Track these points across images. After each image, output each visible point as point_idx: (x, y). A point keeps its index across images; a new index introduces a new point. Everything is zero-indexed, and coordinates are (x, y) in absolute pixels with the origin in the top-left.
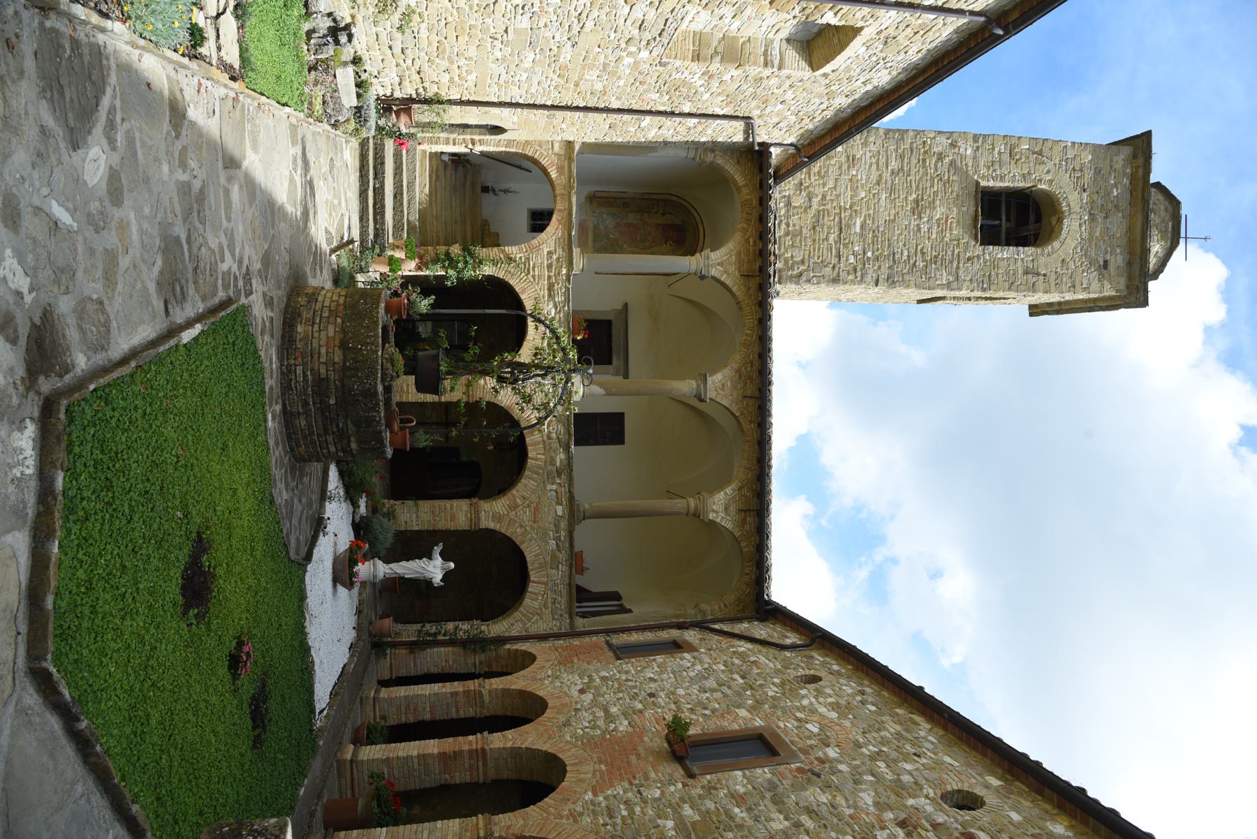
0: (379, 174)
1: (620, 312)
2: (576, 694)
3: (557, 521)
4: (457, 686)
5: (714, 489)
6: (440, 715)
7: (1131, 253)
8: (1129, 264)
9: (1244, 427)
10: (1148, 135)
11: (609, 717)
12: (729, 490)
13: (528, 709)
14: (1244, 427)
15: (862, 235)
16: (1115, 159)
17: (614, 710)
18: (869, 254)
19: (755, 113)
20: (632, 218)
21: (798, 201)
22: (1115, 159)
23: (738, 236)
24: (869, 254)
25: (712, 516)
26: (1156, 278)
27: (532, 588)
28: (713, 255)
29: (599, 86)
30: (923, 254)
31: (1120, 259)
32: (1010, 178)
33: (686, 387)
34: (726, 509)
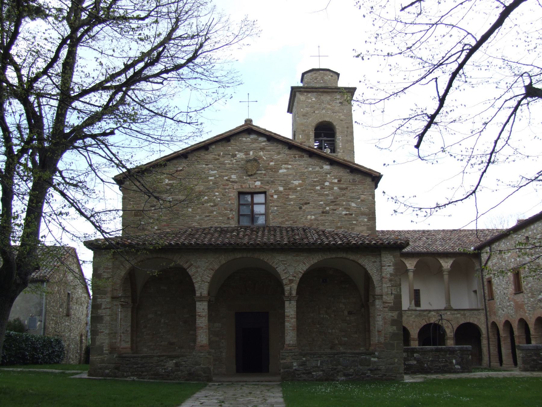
2: (503, 313)
3: (451, 314)
4: (502, 343)
5: (441, 266)
6: (510, 347)
9: (382, 175)
10: (355, 89)
11: (510, 306)
12: (441, 262)
13: (508, 324)
14: (382, 175)
16: (302, 100)
17: (508, 304)
22: (302, 100)
25: (449, 267)
27: (471, 321)
34: (447, 262)
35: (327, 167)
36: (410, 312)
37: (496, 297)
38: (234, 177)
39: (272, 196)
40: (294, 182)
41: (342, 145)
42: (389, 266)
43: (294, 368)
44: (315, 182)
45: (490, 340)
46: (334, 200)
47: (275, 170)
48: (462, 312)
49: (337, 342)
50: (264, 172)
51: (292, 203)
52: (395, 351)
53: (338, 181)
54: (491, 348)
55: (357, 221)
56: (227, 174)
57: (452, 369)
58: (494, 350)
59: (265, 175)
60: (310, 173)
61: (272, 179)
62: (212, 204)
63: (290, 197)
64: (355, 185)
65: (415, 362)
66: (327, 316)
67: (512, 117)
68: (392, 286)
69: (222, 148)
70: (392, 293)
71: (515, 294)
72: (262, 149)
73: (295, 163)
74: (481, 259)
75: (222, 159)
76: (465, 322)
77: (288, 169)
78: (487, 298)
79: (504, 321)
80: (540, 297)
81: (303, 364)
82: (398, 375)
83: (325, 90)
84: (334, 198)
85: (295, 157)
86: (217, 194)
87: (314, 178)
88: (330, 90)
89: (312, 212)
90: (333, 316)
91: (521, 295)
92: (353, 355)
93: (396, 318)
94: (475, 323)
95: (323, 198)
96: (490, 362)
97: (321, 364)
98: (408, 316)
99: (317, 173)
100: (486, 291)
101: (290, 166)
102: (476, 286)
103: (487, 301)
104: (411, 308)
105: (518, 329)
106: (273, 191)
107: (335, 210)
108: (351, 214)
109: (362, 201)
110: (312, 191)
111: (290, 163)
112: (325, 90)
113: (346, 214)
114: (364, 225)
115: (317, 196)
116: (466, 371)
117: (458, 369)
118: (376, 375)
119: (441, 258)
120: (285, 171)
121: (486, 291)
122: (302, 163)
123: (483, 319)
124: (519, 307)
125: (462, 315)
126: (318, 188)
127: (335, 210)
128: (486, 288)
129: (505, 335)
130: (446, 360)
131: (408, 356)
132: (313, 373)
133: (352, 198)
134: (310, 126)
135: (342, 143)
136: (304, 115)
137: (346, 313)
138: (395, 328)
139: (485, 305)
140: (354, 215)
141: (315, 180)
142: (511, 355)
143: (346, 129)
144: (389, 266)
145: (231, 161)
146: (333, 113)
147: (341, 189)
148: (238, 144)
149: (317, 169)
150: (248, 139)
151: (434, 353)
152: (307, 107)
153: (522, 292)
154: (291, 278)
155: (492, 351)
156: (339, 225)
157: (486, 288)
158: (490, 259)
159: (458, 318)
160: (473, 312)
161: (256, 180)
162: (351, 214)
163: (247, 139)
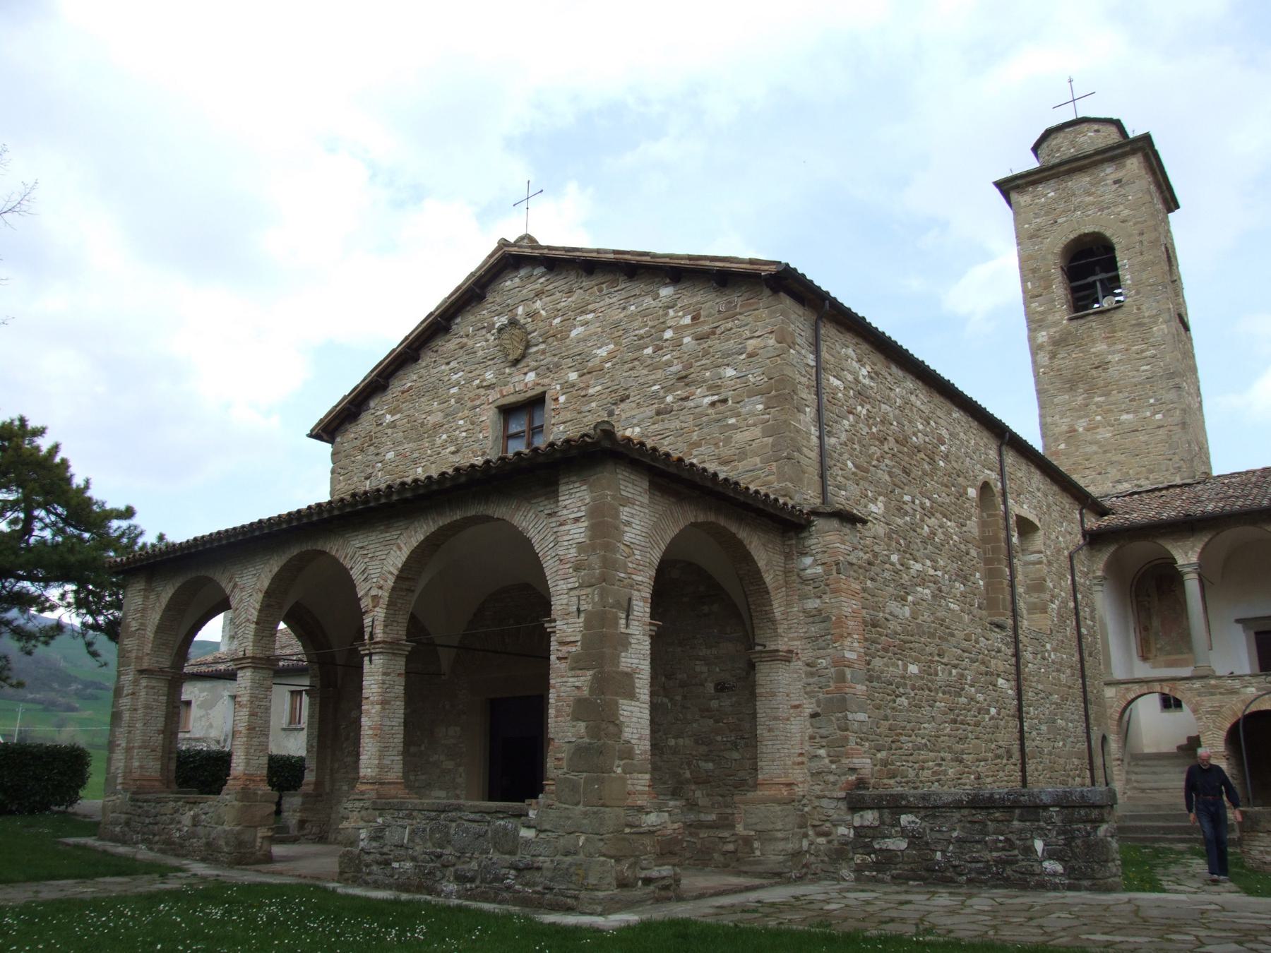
0: (1143, 829)
1: (1246, 629)
7: (1102, 161)
8: (1111, 159)
10: (998, 184)
15: (1135, 412)
16: (1023, 204)
18: (1152, 401)
19: (1066, 553)
20: (1156, 623)
21: (1113, 473)
22: (1023, 204)
23: (1161, 542)
24: (1152, 401)
26: (1117, 124)
29: (1068, 671)
30: (1142, 351)
31: (1109, 170)
32: (1059, 289)
35: (666, 292)
38: (489, 376)
39: (557, 399)
40: (598, 351)
41: (1132, 279)
42: (577, 520)
43: (362, 844)
44: (641, 338)
46: (684, 373)
47: (560, 335)
49: (688, 775)
50: (542, 347)
51: (594, 405)
52: (581, 807)
53: (693, 319)
55: (738, 415)
56: (477, 372)
57: (1033, 874)
59: (543, 352)
60: (631, 318)
61: (556, 359)
62: (453, 449)
63: (591, 391)
64: (733, 317)
65: (903, 845)
66: (666, 700)
68: (581, 586)
69: (472, 318)
70: (579, 611)
72: (539, 294)
73: (602, 304)
75: (470, 343)
77: (586, 323)
81: (377, 836)
82: (583, 894)
83: (1074, 165)
84: (685, 368)
85: (600, 291)
86: (461, 422)
87: (639, 329)
88: (1087, 161)
89: (633, 417)
90: (678, 698)
92: (477, 817)
93: (586, 692)
95: (659, 374)
97: (411, 840)
99: (644, 313)
101: (590, 316)
106: (558, 387)
107: (686, 399)
108: (725, 401)
109: (750, 356)
110: (636, 363)
111: (590, 307)
112: (1074, 165)
113: (713, 404)
114: (754, 425)
115: (645, 372)
116: (1086, 883)
117: (1055, 874)
118: (527, 884)
120: (581, 329)
122: (614, 300)
126: (649, 351)
127: (686, 399)
130: (1007, 840)
131: (882, 823)
132: (396, 865)
133: (726, 355)
134: (1050, 257)
135: (1132, 273)
136: (1031, 237)
137: (710, 687)
138: (582, 725)
140: (730, 402)
141: (642, 332)
143: (1138, 238)
144: (577, 520)
145: (487, 341)
146: (1101, 210)
147: (699, 338)
148: (498, 300)
149: (648, 301)
150: (517, 280)
151: (965, 812)
152: (1037, 216)
154: (373, 592)
156: (695, 437)
161: (526, 370)
162: (725, 401)
163: (510, 283)
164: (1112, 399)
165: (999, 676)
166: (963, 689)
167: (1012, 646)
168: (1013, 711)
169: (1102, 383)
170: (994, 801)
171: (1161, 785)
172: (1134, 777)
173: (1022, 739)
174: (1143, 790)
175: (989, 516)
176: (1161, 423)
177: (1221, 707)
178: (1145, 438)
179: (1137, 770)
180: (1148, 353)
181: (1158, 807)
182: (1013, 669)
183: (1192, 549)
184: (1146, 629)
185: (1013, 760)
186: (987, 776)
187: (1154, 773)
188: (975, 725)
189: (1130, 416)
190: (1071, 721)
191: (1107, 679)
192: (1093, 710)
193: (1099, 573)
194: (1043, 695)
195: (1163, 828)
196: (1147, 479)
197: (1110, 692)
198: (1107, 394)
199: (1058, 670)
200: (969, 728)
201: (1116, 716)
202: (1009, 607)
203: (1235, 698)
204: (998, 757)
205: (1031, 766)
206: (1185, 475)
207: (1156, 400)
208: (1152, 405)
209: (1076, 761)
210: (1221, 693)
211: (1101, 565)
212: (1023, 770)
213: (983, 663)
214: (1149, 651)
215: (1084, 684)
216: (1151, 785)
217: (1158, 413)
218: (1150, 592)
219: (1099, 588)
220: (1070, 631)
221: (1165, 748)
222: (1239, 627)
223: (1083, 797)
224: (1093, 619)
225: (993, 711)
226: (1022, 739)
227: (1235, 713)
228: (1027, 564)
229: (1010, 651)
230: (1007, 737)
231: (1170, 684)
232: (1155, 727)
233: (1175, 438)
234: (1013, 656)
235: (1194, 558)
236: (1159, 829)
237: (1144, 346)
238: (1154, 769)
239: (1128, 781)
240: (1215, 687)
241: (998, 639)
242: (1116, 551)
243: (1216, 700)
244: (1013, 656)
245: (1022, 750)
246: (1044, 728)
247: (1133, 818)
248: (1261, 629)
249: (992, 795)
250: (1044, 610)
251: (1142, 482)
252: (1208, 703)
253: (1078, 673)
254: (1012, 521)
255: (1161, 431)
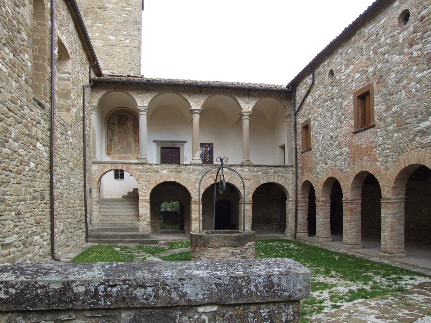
12: (240, 102)
15: (116, 36)
17: (337, 152)
19: (82, 84)
20: (116, 138)
23: (131, 93)
24: (125, 33)
25: (250, 109)
27: (276, 181)
28: (139, 105)
29: (78, 151)
30: (125, 7)
33: (196, 118)
34: (248, 103)
36: (192, 167)
37: (315, 145)
45: (299, 204)
48: (264, 169)
54: (299, 214)
58: (303, 217)
67: (308, 80)
71: (355, 133)
74: (295, 100)
76: (268, 182)
78: (300, 151)
79: (325, 179)
80: (426, 124)
91: (369, 133)
94: (281, 183)
96: (296, 232)
98: (188, 172)
100: (300, 142)
102: (285, 137)
103: (299, 154)
104: (193, 162)
105: (353, 189)
119: (239, 97)
121: (300, 142)
123: (291, 178)
124: (358, 153)
125: (264, 173)
128: (299, 137)
129: (324, 199)
139: (296, 160)
142: (329, 225)
153: (374, 126)
155: (300, 218)
157: (299, 137)
158: (311, 93)
159: (258, 176)
160: (278, 169)
164: (105, 26)
165: (38, 140)
166: (7, 142)
167: (49, 123)
168: (46, 167)
169: (101, 17)
170: (75, 297)
171: (114, 214)
172: (102, 210)
173: (52, 187)
174: (107, 216)
175: (39, 24)
176: (128, 45)
177: (150, 178)
178: (120, 50)
179: (103, 206)
180: (127, 9)
181: (115, 225)
182: (48, 139)
183: (146, 99)
184: (111, 140)
185: (45, 201)
186: (26, 213)
187: (112, 208)
188: (17, 173)
189: (113, 38)
190: (77, 180)
191: (94, 160)
192: (87, 174)
193: (95, 104)
194: (64, 161)
195: (121, 236)
196: (117, 70)
197: (95, 167)
198: (104, 24)
199: (73, 149)
200: (12, 175)
201: (97, 180)
202: (49, 95)
203: (157, 175)
204: (35, 198)
205: (56, 205)
206: (136, 72)
207: (128, 33)
208: (125, 35)
209: (79, 202)
210: (151, 172)
211: (97, 100)
212: (52, 207)
213: (26, 126)
214: (111, 151)
215: (84, 160)
216: (112, 214)
217: (127, 39)
218: (120, 122)
219: (94, 112)
220: (80, 128)
221: (114, 197)
222: (155, 144)
223: (270, 285)
224: (90, 127)
225: (32, 165)
226: (52, 187)
227: (156, 182)
228: (60, 79)
229: (47, 126)
230: (41, 185)
231: (126, 165)
232: (112, 187)
233: (134, 54)
234: (49, 130)
235: (146, 104)
236: (119, 236)
237: (126, 5)
238: (112, 206)
239: (100, 212)
240: (149, 169)
241: (38, 113)
242: (106, 94)
243: (149, 175)
244: (49, 130)
245: (51, 194)
246: (64, 181)
247: (103, 230)
248: (164, 146)
249: (67, 285)
250: (68, 110)
251: (115, 71)
252: (144, 176)
253: (82, 154)
254: (56, 42)
255: (128, 49)
